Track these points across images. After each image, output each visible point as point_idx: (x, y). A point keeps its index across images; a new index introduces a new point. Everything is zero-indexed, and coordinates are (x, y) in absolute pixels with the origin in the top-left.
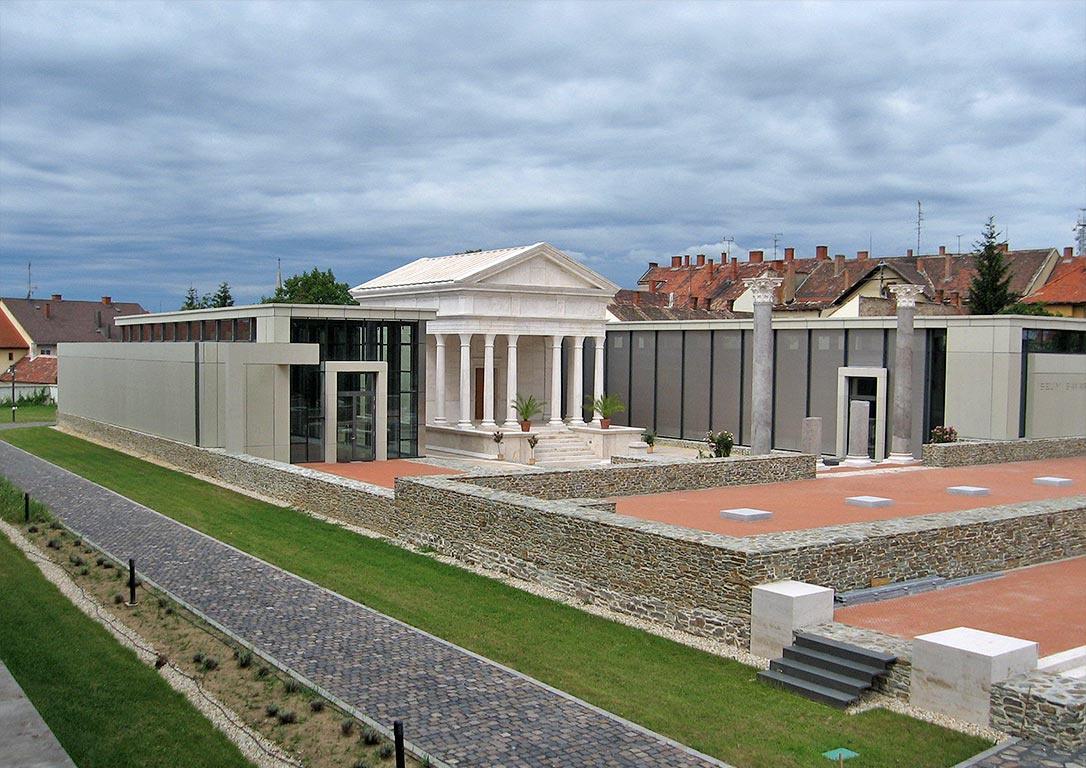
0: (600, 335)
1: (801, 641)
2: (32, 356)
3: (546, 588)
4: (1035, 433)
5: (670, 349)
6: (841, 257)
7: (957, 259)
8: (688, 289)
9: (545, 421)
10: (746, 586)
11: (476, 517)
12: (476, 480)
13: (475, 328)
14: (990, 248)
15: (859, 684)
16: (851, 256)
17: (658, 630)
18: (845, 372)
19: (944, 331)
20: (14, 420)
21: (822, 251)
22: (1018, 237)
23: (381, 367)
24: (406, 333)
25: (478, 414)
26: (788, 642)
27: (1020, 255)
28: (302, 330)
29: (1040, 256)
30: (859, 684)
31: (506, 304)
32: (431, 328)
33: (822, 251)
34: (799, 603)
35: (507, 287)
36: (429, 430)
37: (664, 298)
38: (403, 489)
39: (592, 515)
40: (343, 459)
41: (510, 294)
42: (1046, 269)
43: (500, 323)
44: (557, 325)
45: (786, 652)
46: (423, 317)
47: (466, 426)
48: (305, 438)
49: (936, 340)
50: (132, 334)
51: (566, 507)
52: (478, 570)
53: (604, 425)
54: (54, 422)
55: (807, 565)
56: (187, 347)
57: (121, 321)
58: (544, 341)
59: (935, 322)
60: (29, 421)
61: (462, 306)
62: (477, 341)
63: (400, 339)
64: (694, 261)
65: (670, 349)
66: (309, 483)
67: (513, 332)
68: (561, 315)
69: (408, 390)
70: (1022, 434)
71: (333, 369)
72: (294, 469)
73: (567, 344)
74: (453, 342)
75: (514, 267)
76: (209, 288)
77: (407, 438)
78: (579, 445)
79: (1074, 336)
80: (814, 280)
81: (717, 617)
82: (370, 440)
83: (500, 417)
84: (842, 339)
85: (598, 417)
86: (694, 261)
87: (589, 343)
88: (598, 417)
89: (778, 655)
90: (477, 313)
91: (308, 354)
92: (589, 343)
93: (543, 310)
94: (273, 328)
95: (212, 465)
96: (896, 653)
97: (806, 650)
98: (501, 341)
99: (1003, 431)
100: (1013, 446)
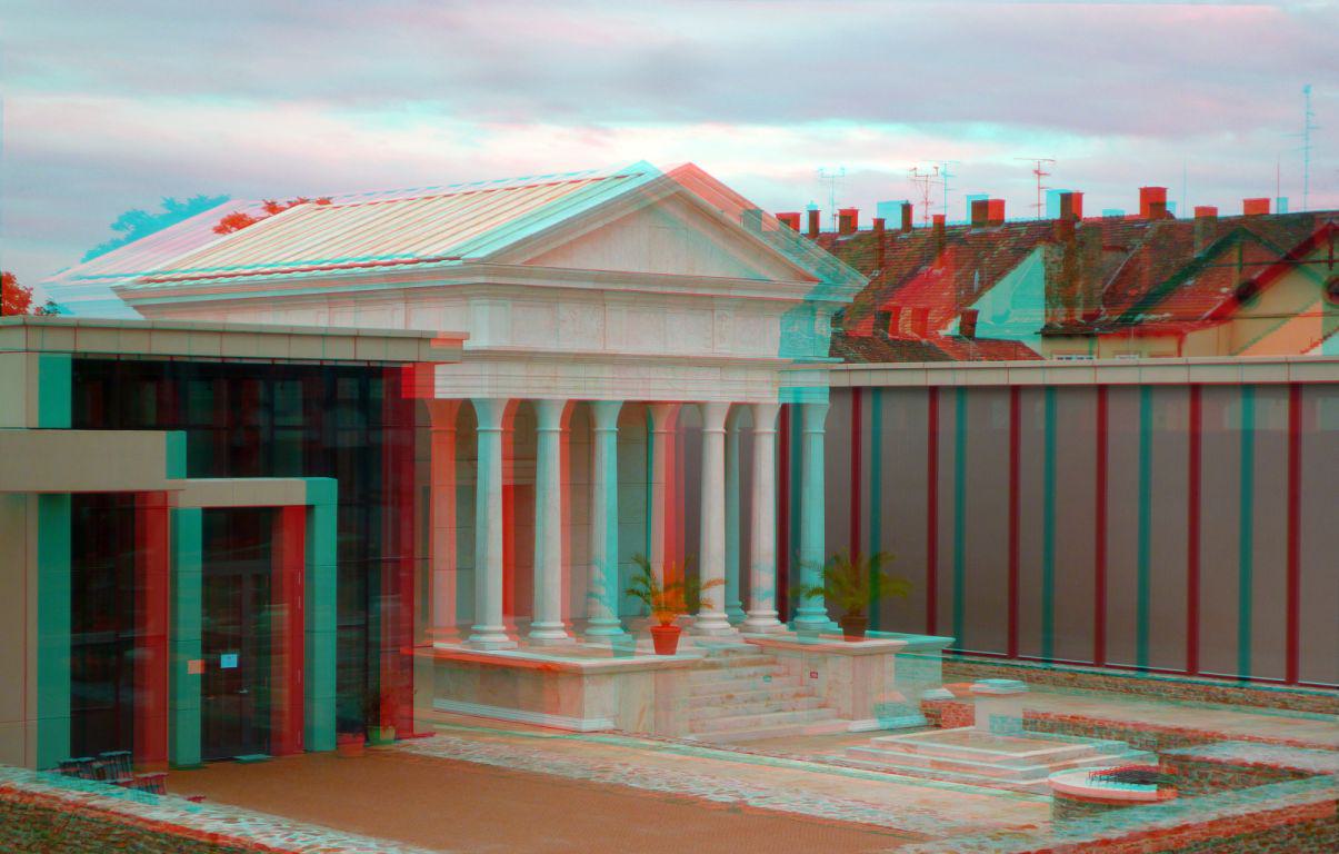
6: (1207, 215)
13: (517, 384)
20: (1292, 678)
25: (519, 604)
33: (1154, 199)
35: (599, 276)
36: (445, 662)
41: (601, 293)
43: (580, 371)
44: (714, 374)
46: (425, 354)
47: (495, 641)
48: (107, 729)
59: (867, 374)
61: (484, 327)
62: (523, 416)
64: (829, 224)
68: (725, 349)
69: (382, 563)
72: (73, 791)
75: (610, 225)
79: (288, 397)
86: (829, 224)
90: (613, 347)
92: (790, 419)
93: (682, 335)
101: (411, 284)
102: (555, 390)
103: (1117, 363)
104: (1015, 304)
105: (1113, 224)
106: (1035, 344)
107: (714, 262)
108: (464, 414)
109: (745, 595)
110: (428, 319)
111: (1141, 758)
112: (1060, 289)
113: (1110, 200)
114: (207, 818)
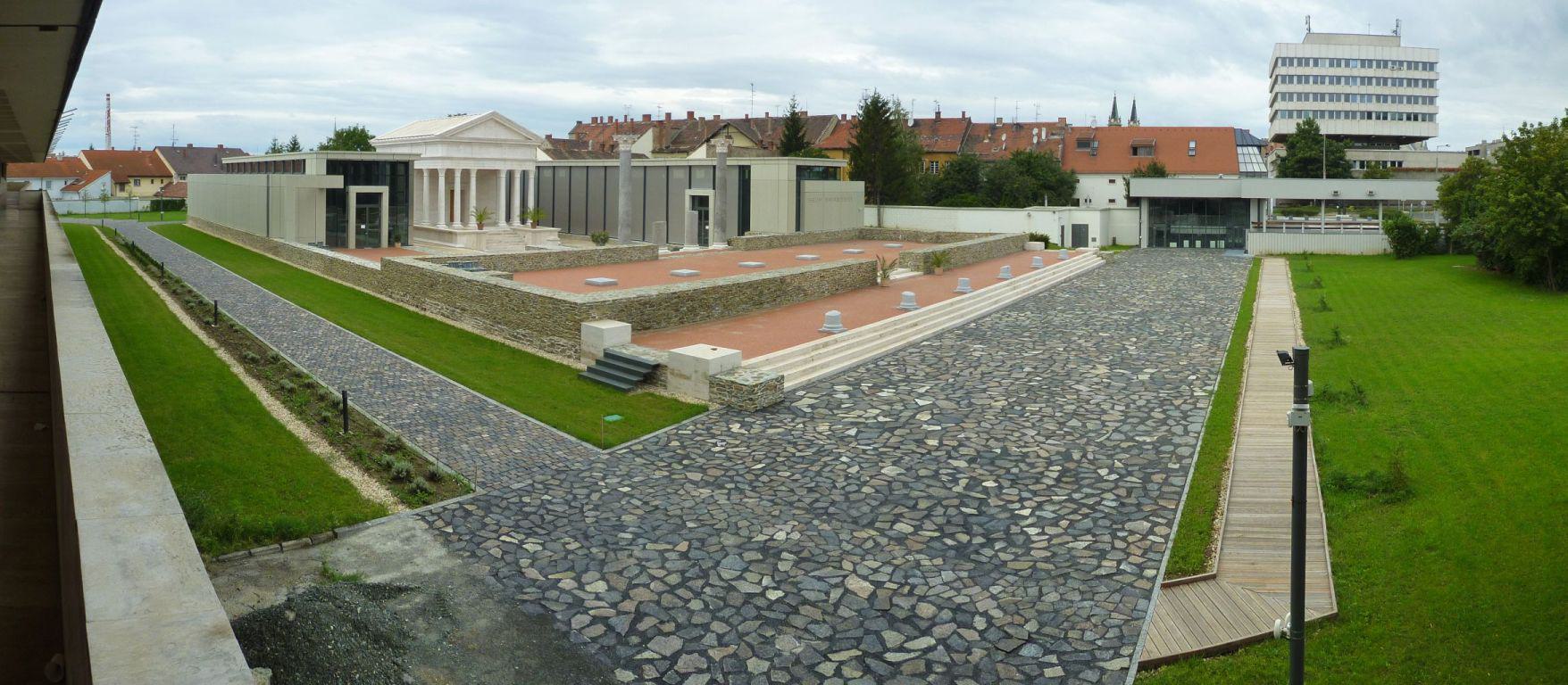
0: (531, 168)
1: (607, 355)
2: (175, 181)
3: (467, 325)
4: (810, 225)
5: (579, 177)
6: (702, 119)
7: (776, 120)
8: (601, 139)
9: (495, 224)
10: (578, 323)
11: (428, 283)
12: (432, 260)
13: (449, 165)
14: (794, 114)
15: (635, 379)
16: (709, 117)
17: (530, 350)
18: (689, 193)
19: (749, 167)
21: (691, 114)
22: (814, 107)
23: (384, 190)
24: (1282, 70)
26: (601, 355)
27: (815, 118)
28: (333, 167)
29: (825, 120)
30: (635, 379)
31: (468, 149)
32: (417, 165)
34: (613, 335)
37: (585, 144)
38: (385, 264)
39: (493, 281)
40: (359, 245)
41: (470, 143)
42: (831, 127)
45: (598, 362)
47: (442, 226)
48: (335, 237)
49: (744, 172)
50: (231, 168)
51: (480, 276)
52: (428, 314)
53: (533, 226)
54: (185, 219)
55: (619, 311)
56: (263, 176)
57: (225, 161)
58: (495, 173)
60: (171, 218)
61: (439, 151)
62: (450, 174)
63: (398, 174)
65: (579, 177)
66: (332, 260)
67: (474, 167)
69: (401, 201)
70: (798, 228)
71: (354, 190)
73: (510, 174)
74: (434, 174)
76: (285, 141)
77: (398, 237)
78: (511, 238)
80: (678, 135)
81: (562, 342)
82: (378, 235)
83: (464, 220)
84: (641, 173)
85: (530, 221)
87: (524, 174)
88: (530, 221)
89: (593, 364)
91: (337, 182)
92: (524, 174)
93: (493, 153)
94: (316, 168)
95: (276, 248)
96: (660, 361)
97: (611, 361)
98: (466, 173)
99: (785, 226)
100: (792, 237)
101: (413, 143)
102: (458, 167)
103: (672, 160)
104: (645, 143)
105: (677, 122)
106: (649, 155)
107: (503, 135)
108: (421, 171)
109: (508, 218)
110: (415, 150)
111: (535, 263)
112: (658, 139)
113: (680, 114)
114: (358, 261)
